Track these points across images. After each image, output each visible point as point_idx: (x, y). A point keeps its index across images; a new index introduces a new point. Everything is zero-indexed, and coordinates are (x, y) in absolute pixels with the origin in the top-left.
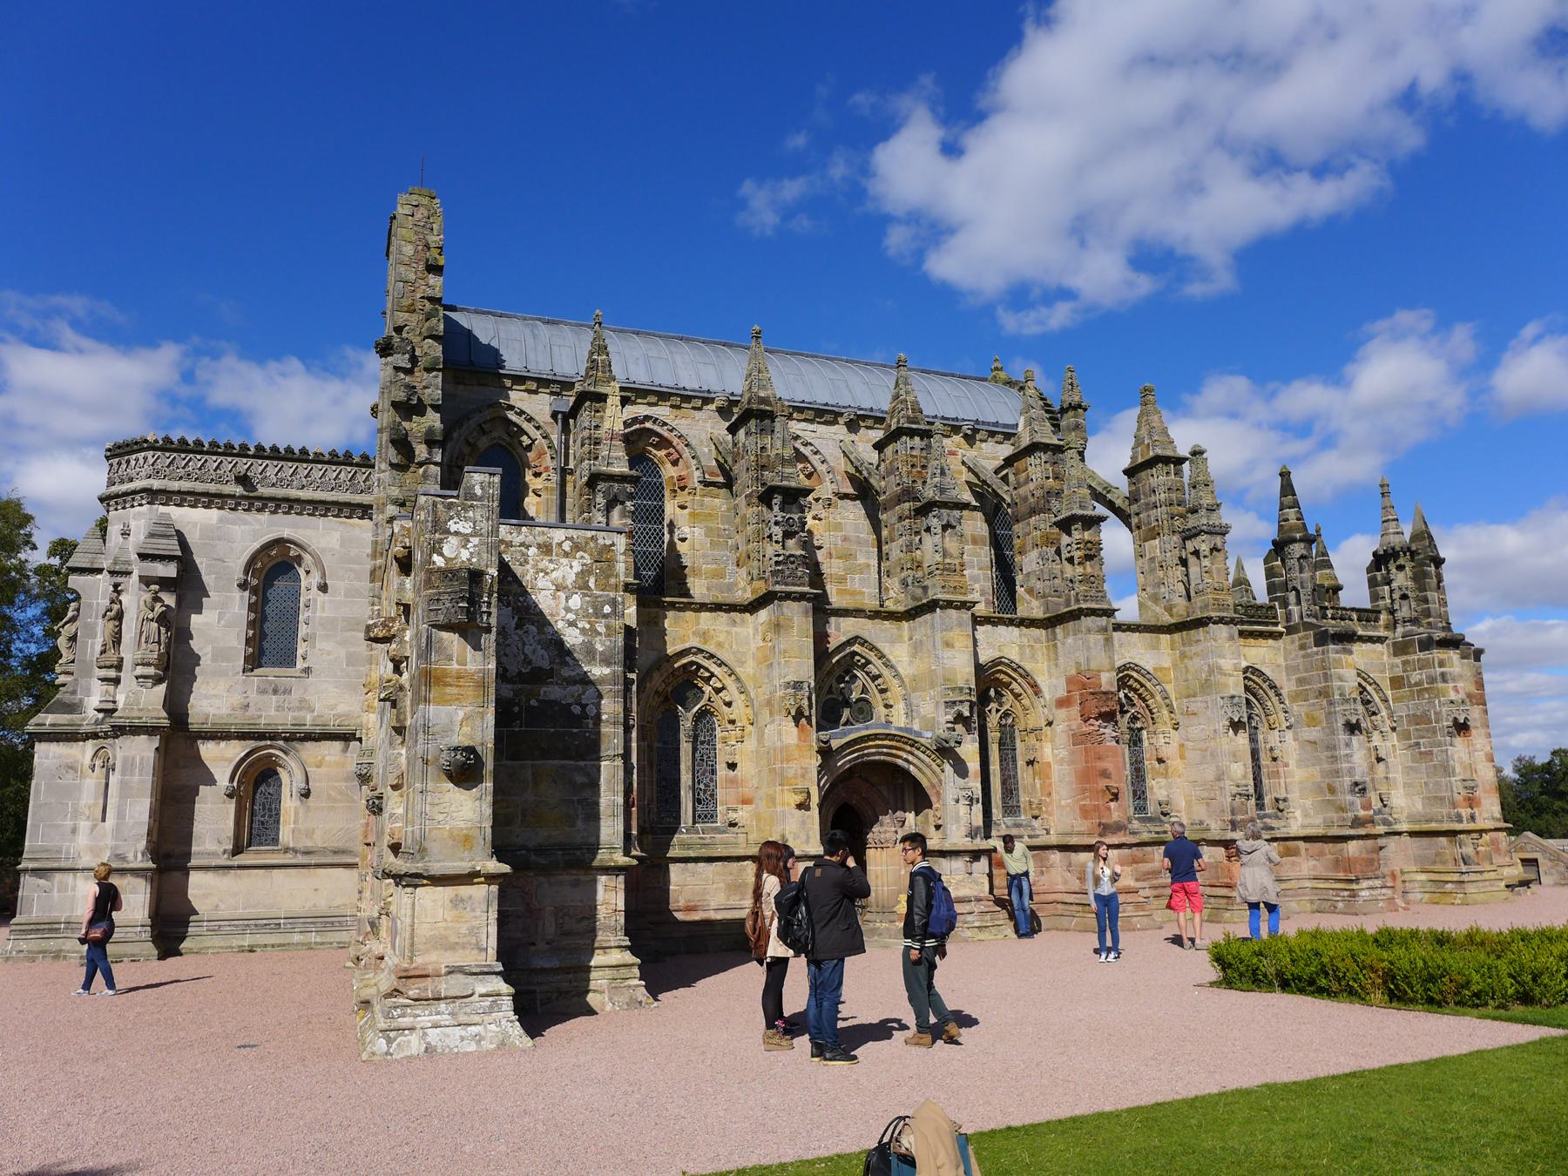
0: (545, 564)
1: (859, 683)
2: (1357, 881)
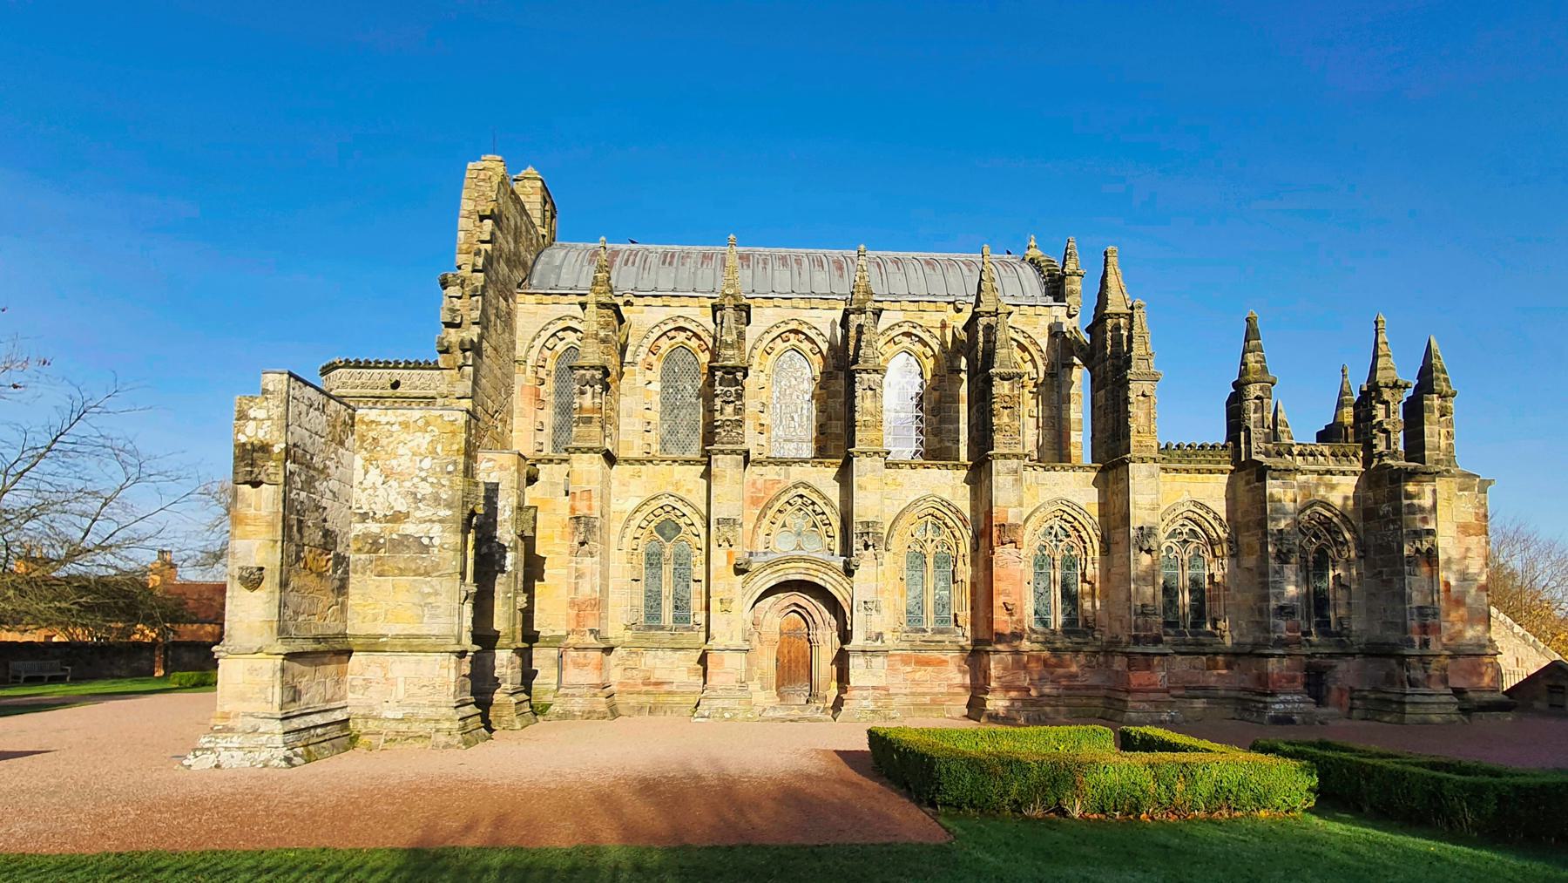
0: (404, 436)
2: (1273, 694)
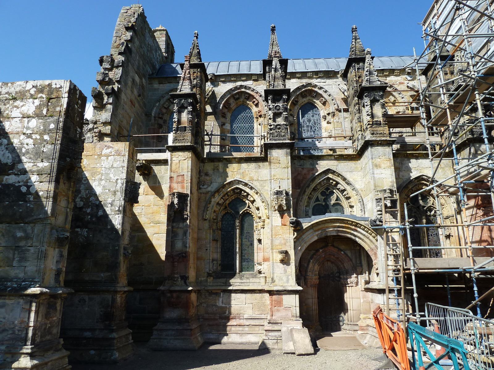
1: (335, 195)
